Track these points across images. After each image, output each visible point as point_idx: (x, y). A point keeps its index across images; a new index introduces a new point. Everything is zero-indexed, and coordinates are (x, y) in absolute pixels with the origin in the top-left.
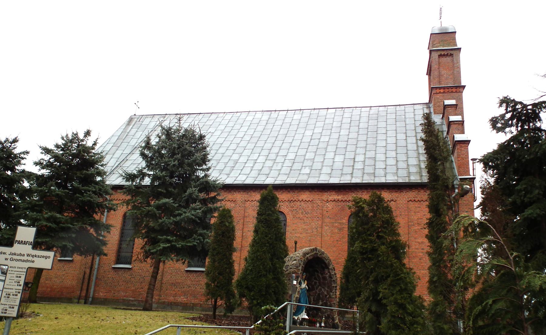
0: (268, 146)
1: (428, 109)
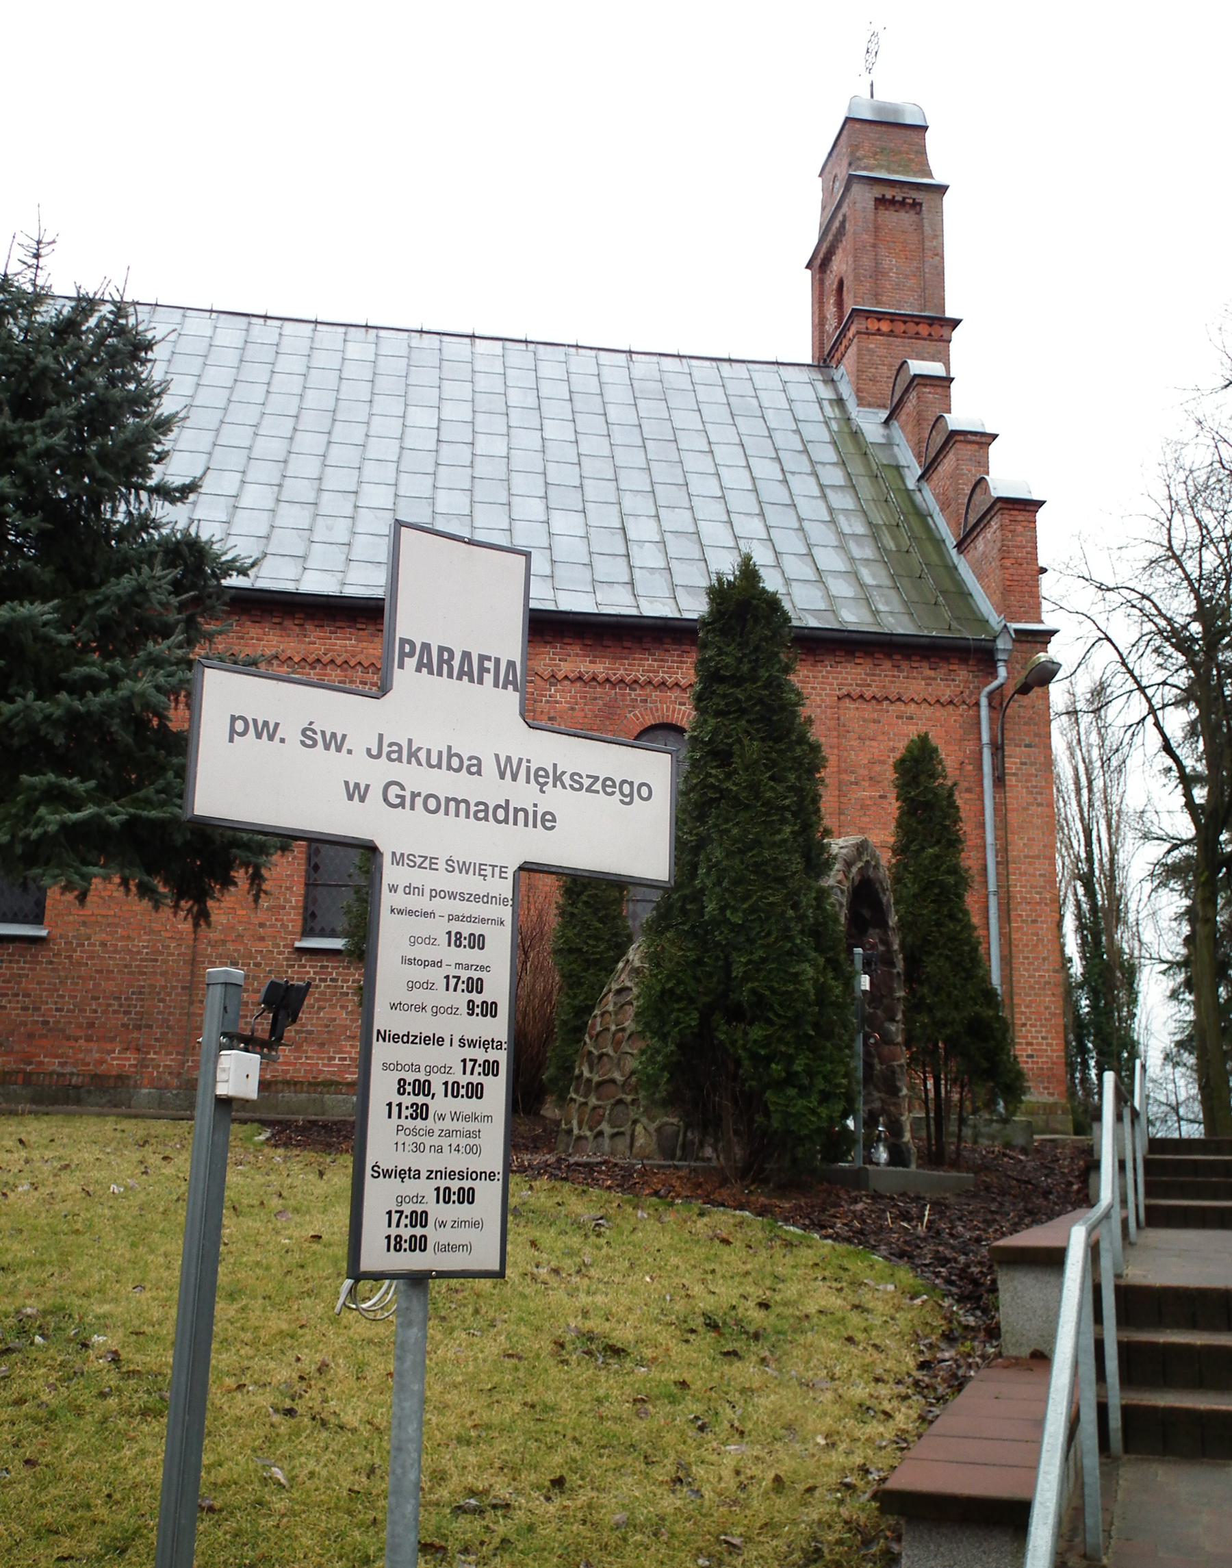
0: (269, 447)
1: (830, 386)
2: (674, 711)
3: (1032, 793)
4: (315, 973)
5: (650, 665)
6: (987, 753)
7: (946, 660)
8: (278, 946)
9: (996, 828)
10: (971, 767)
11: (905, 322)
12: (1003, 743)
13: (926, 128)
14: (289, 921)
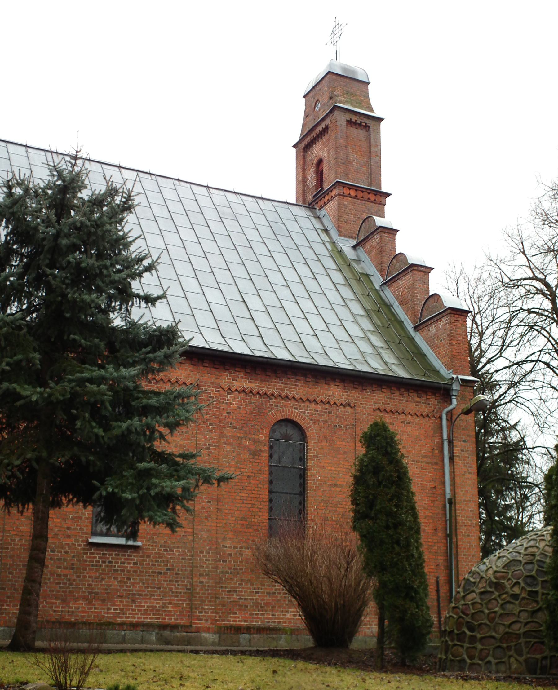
2: (292, 413)
3: (466, 466)
4: (99, 558)
5: (280, 386)
6: (446, 444)
7: (426, 393)
8: (78, 541)
9: (451, 485)
10: (437, 451)
11: (363, 192)
12: (453, 440)
13: (368, 83)
14: (84, 526)
